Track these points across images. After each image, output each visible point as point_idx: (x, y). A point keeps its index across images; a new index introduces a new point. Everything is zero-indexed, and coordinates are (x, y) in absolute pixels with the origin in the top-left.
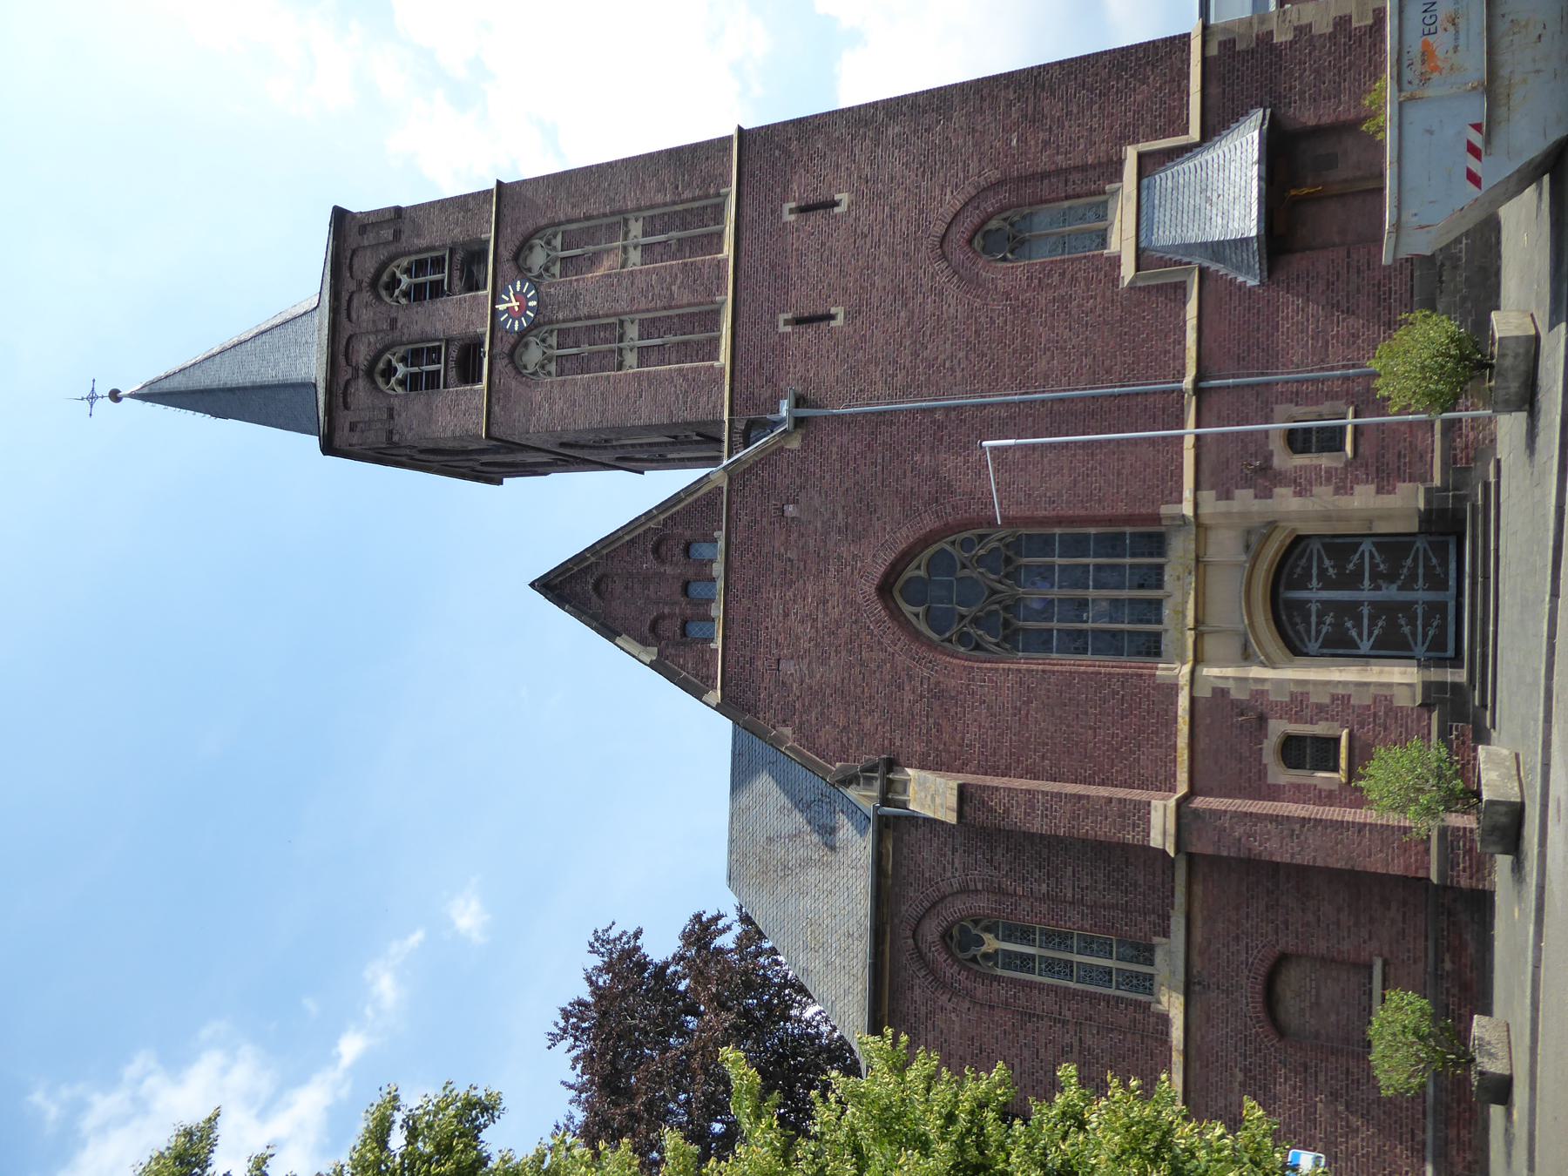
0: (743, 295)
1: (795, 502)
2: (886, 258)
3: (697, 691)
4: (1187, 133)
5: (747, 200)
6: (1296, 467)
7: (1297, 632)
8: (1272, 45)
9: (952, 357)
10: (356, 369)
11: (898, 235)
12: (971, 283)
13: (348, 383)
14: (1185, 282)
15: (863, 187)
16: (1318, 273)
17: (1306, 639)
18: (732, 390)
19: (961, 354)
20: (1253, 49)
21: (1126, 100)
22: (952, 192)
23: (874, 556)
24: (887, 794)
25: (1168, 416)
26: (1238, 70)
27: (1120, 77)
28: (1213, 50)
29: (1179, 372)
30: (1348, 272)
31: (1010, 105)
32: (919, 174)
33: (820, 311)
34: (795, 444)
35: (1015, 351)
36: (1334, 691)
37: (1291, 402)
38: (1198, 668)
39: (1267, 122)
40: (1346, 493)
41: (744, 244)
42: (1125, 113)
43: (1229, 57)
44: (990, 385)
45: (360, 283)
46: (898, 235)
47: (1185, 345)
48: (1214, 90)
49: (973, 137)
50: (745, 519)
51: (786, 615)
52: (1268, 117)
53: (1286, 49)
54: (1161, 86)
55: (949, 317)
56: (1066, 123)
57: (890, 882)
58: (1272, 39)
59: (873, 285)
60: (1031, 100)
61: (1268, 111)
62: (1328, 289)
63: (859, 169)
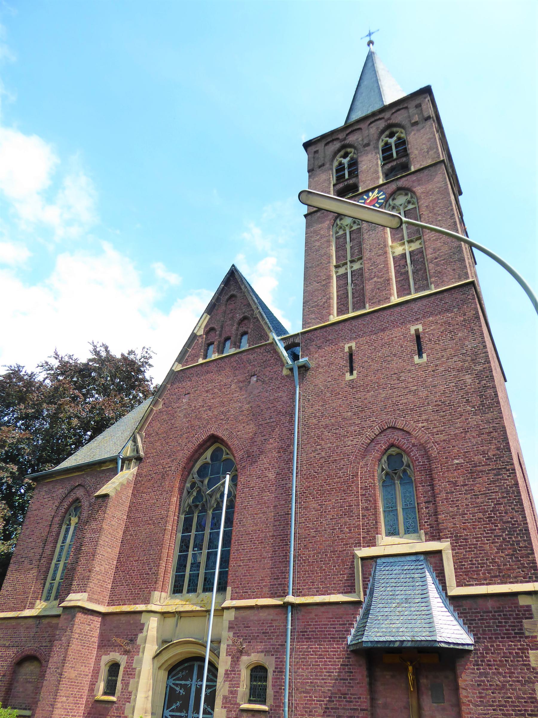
0: (368, 318)
1: (257, 381)
2: (384, 395)
3: (180, 359)
4: (458, 586)
5: (425, 302)
6: (240, 671)
7: (177, 673)
8: (527, 649)
9: (322, 449)
10: (345, 139)
11: (398, 399)
12: (366, 451)
13: (337, 139)
14: (355, 592)
15: (430, 369)
16: (352, 687)
17: (175, 678)
18: (316, 329)
19: (323, 454)
20: (523, 633)
21: (485, 537)
22: (423, 427)
23: (227, 429)
24: (127, 460)
25: (277, 587)
26: (506, 622)
27: (503, 530)
28: (523, 601)
29: (301, 592)
30: (351, 709)
31: (484, 453)
32: (437, 403)
33: (355, 365)
34: (285, 372)
35: (322, 486)
36: (133, 694)
37: (276, 668)
38: (158, 615)
39: (446, 646)
40: (223, 704)
41: (398, 309)
42: (476, 538)
43: (517, 615)
44: (305, 475)
45: (389, 119)
46: (398, 399)
47: (316, 595)
48: (490, 604)
49: (462, 433)
50: (251, 357)
51: (207, 392)
52: (466, 647)
53: (523, 661)
54: (496, 562)
55: (345, 442)
56: (469, 496)
57: (99, 470)
58: (531, 649)
59: (368, 391)
60: (487, 468)
61: (472, 648)
62: (342, 694)
63: (443, 363)
